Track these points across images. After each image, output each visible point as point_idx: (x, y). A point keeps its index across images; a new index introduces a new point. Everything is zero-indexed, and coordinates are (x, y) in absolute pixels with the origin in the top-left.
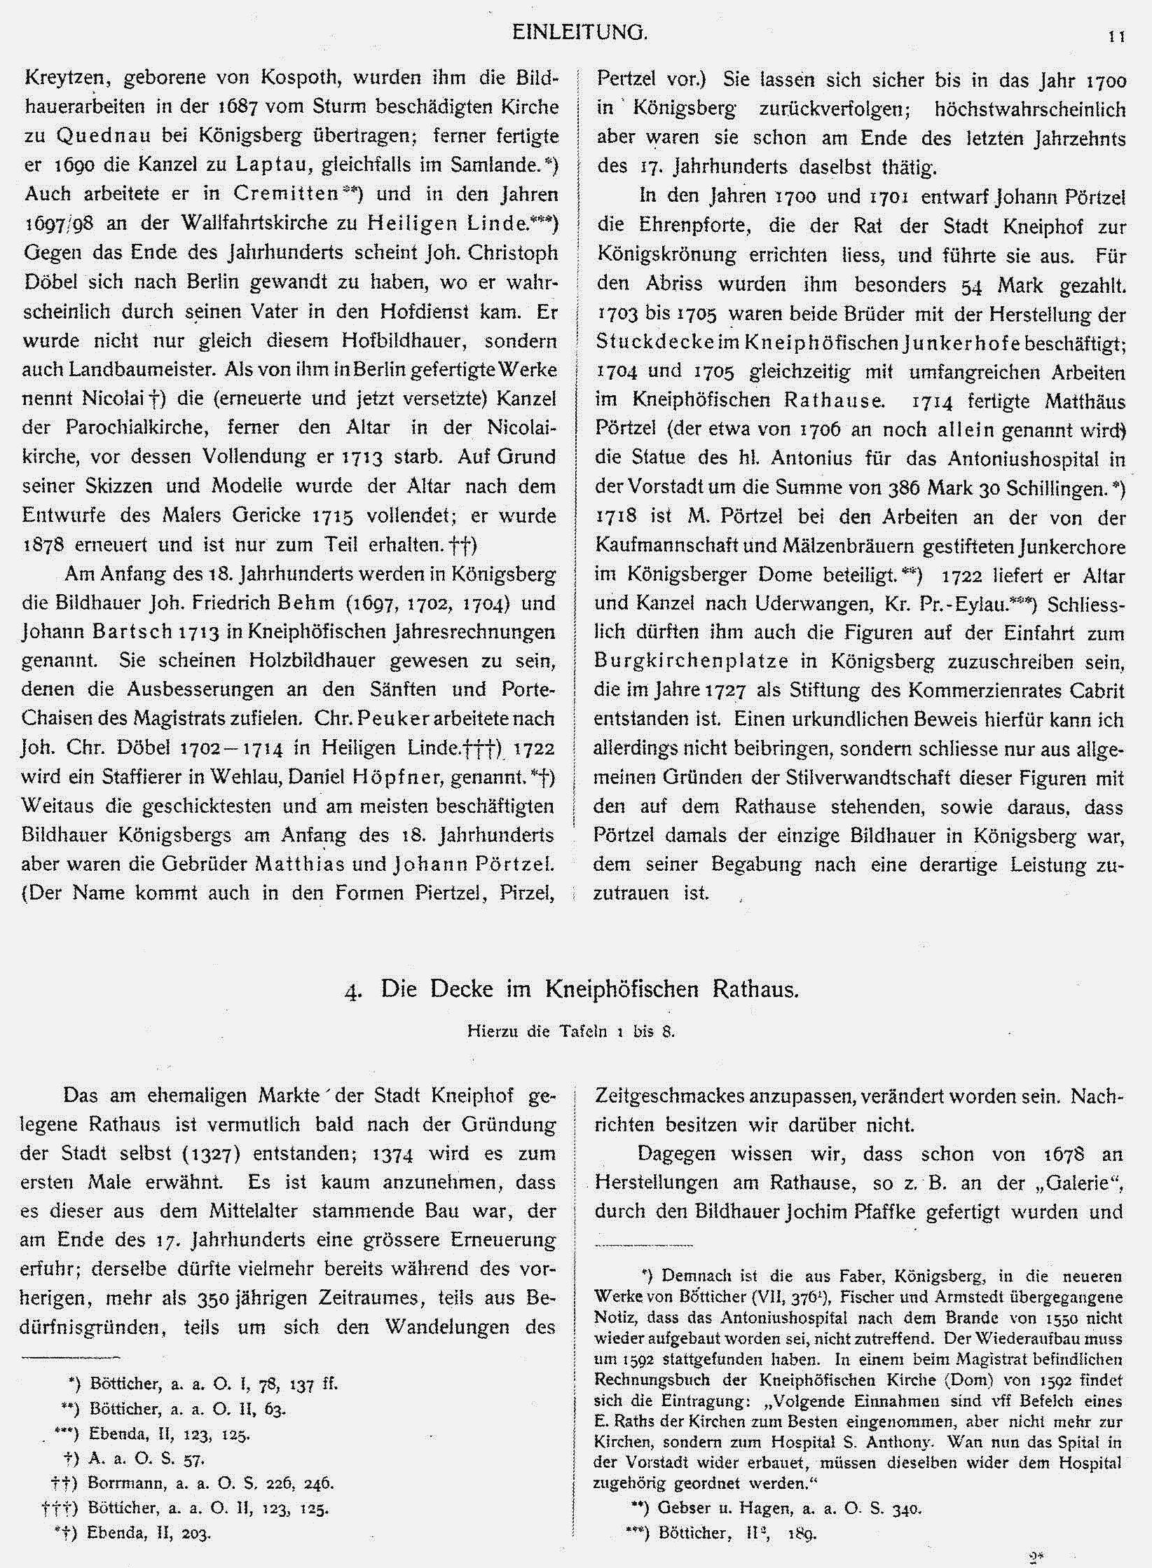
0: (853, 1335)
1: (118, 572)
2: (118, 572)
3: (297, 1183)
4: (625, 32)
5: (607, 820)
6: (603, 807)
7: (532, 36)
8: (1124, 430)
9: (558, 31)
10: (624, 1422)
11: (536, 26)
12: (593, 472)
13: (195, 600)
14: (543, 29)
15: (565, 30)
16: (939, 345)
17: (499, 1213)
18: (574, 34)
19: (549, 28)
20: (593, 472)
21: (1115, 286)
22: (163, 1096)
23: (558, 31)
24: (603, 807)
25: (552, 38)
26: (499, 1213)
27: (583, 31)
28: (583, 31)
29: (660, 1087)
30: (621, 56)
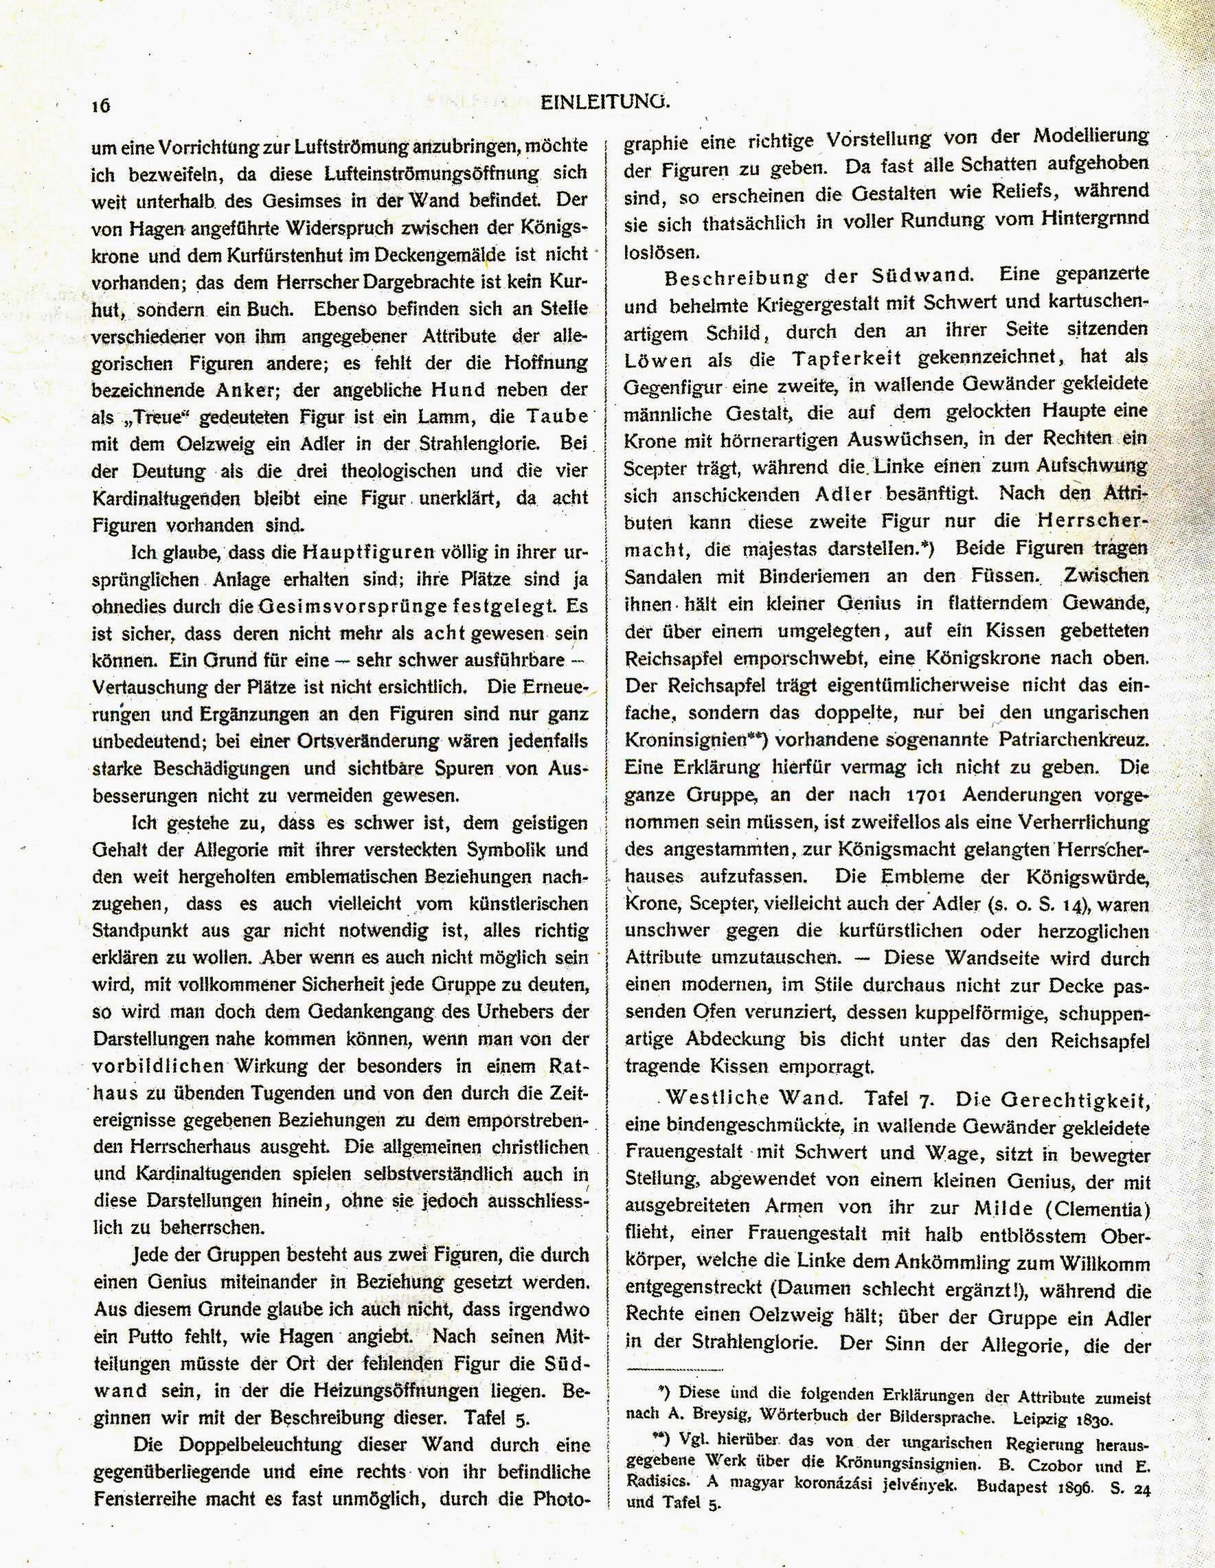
1: (229, 578)
2: (229, 578)
5: (571, 159)
6: (635, 850)
7: (560, 105)
9: (584, 102)
11: (563, 97)
12: (589, 1026)
13: (751, 1230)
14: (565, 104)
18: (599, 103)
19: (575, 99)
20: (589, 1026)
22: (936, 931)
24: (635, 850)
27: (608, 101)
30: (646, 124)
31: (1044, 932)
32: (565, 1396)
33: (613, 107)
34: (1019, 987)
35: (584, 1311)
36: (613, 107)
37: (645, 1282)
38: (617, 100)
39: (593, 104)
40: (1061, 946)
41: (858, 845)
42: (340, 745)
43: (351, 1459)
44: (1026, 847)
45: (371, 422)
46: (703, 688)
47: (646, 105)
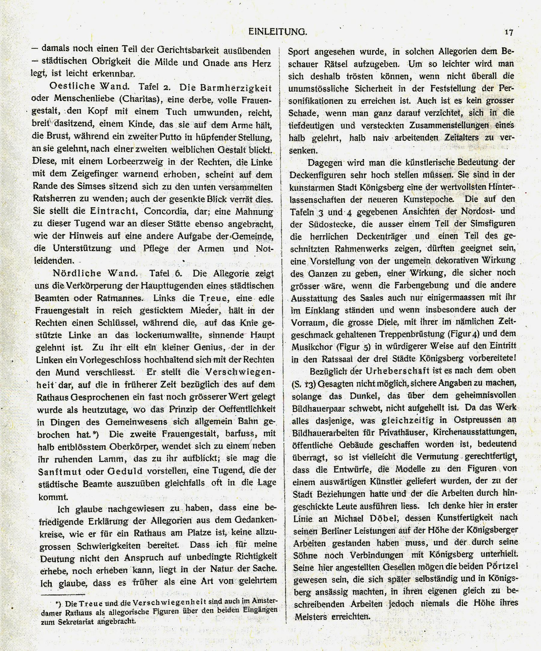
0: (376, 382)
3: (436, 469)
4: (294, 31)
8: (221, 482)
9: (268, 31)
10: (38, 186)
11: (258, 29)
14: (260, 32)
15: (271, 31)
16: (190, 603)
17: (121, 224)
18: (275, 32)
19: (264, 30)
21: (511, 125)
23: (268, 31)
25: (266, 34)
26: (121, 224)
27: (279, 31)
28: (279, 31)
29: (338, 48)
30: (297, 42)
31: (188, 508)
32: (84, 486)
33: (281, 34)
34: (174, 509)
35: (143, 410)
36: (281, 34)
37: (502, 185)
38: (283, 31)
39: (272, 32)
40: (207, 453)
41: (497, 576)
42: (467, 262)
43: (392, 255)
44: (225, 555)
45: (60, 75)
46: (261, 114)
47: (296, 34)
